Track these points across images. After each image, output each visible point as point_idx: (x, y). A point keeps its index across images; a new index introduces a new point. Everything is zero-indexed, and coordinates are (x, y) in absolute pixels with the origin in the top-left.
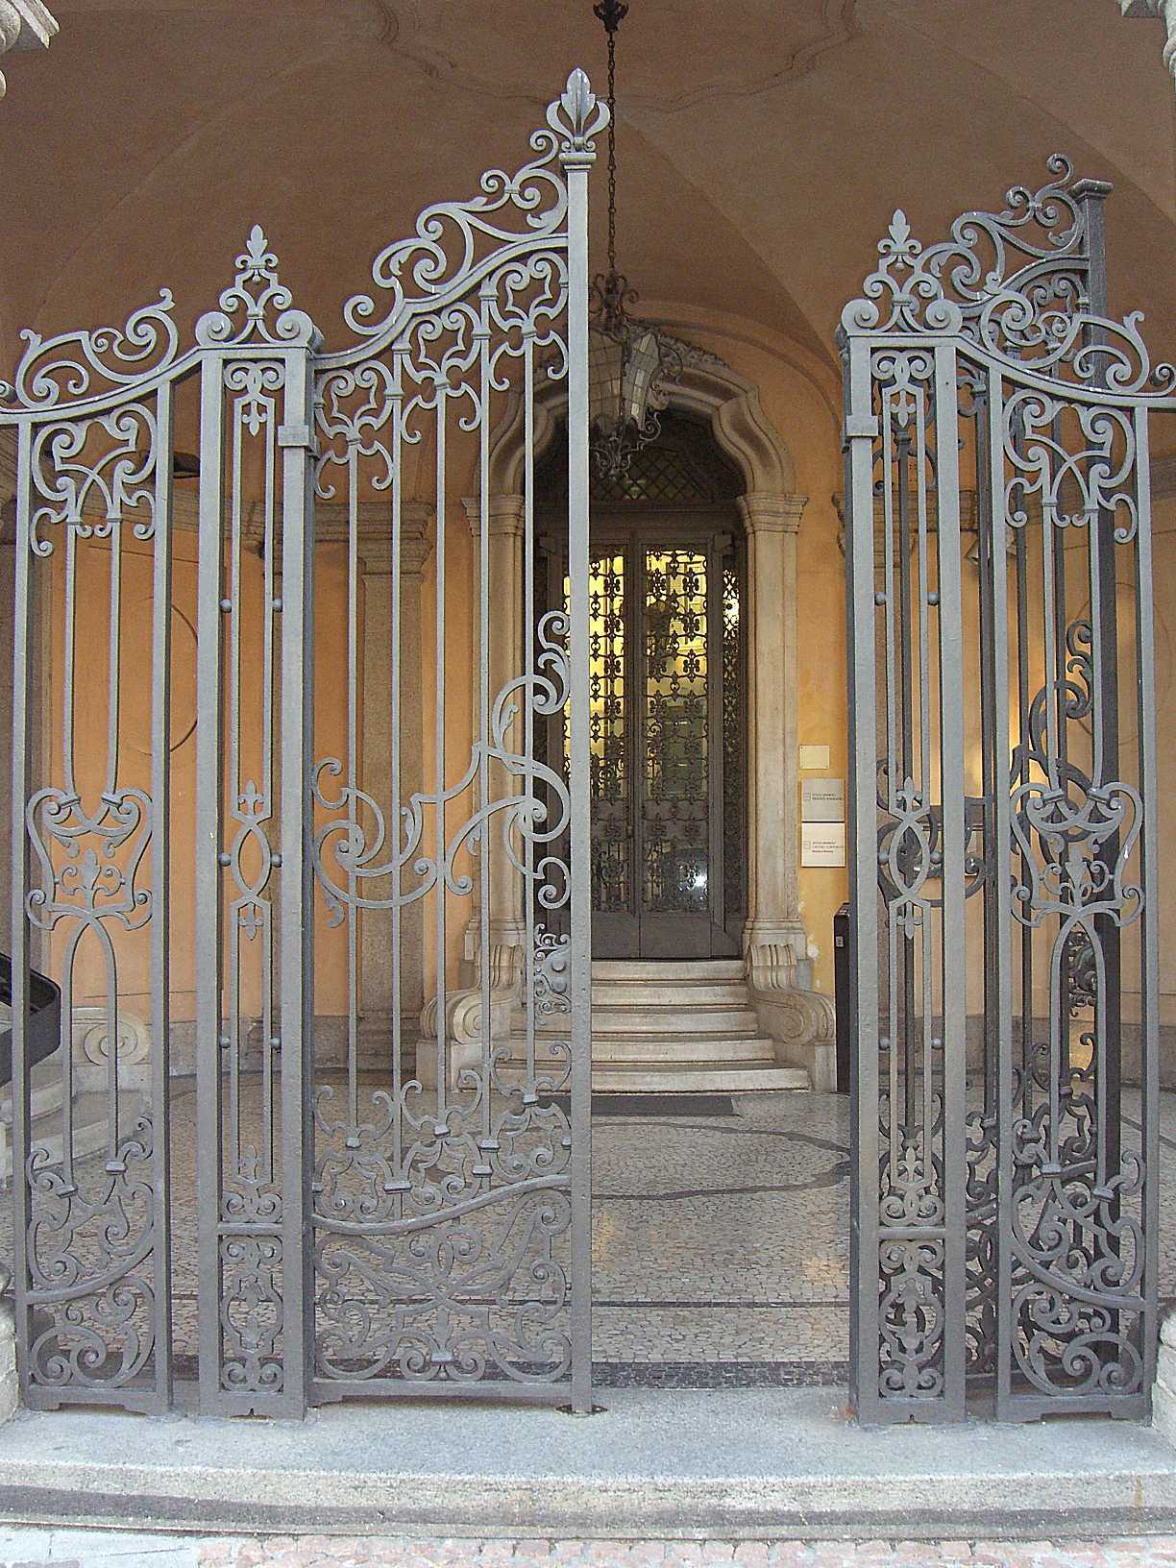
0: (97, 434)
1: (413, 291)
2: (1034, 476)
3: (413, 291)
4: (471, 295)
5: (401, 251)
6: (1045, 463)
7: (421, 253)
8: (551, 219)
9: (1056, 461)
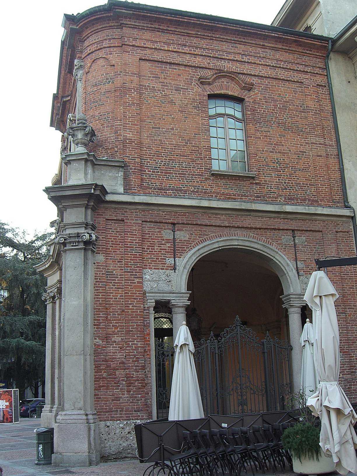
2: (160, 358)
4: (230, 338)
6: (161, 357)
8: (236, 330)
9: (162, 357)
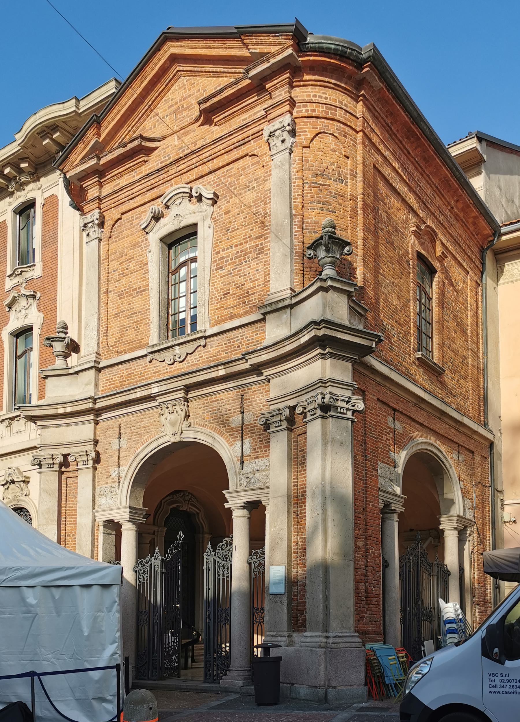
0: (224, 565)
1: (222, 549)
3: (222, 549)
5: (221, 544)
7: (223, 545)
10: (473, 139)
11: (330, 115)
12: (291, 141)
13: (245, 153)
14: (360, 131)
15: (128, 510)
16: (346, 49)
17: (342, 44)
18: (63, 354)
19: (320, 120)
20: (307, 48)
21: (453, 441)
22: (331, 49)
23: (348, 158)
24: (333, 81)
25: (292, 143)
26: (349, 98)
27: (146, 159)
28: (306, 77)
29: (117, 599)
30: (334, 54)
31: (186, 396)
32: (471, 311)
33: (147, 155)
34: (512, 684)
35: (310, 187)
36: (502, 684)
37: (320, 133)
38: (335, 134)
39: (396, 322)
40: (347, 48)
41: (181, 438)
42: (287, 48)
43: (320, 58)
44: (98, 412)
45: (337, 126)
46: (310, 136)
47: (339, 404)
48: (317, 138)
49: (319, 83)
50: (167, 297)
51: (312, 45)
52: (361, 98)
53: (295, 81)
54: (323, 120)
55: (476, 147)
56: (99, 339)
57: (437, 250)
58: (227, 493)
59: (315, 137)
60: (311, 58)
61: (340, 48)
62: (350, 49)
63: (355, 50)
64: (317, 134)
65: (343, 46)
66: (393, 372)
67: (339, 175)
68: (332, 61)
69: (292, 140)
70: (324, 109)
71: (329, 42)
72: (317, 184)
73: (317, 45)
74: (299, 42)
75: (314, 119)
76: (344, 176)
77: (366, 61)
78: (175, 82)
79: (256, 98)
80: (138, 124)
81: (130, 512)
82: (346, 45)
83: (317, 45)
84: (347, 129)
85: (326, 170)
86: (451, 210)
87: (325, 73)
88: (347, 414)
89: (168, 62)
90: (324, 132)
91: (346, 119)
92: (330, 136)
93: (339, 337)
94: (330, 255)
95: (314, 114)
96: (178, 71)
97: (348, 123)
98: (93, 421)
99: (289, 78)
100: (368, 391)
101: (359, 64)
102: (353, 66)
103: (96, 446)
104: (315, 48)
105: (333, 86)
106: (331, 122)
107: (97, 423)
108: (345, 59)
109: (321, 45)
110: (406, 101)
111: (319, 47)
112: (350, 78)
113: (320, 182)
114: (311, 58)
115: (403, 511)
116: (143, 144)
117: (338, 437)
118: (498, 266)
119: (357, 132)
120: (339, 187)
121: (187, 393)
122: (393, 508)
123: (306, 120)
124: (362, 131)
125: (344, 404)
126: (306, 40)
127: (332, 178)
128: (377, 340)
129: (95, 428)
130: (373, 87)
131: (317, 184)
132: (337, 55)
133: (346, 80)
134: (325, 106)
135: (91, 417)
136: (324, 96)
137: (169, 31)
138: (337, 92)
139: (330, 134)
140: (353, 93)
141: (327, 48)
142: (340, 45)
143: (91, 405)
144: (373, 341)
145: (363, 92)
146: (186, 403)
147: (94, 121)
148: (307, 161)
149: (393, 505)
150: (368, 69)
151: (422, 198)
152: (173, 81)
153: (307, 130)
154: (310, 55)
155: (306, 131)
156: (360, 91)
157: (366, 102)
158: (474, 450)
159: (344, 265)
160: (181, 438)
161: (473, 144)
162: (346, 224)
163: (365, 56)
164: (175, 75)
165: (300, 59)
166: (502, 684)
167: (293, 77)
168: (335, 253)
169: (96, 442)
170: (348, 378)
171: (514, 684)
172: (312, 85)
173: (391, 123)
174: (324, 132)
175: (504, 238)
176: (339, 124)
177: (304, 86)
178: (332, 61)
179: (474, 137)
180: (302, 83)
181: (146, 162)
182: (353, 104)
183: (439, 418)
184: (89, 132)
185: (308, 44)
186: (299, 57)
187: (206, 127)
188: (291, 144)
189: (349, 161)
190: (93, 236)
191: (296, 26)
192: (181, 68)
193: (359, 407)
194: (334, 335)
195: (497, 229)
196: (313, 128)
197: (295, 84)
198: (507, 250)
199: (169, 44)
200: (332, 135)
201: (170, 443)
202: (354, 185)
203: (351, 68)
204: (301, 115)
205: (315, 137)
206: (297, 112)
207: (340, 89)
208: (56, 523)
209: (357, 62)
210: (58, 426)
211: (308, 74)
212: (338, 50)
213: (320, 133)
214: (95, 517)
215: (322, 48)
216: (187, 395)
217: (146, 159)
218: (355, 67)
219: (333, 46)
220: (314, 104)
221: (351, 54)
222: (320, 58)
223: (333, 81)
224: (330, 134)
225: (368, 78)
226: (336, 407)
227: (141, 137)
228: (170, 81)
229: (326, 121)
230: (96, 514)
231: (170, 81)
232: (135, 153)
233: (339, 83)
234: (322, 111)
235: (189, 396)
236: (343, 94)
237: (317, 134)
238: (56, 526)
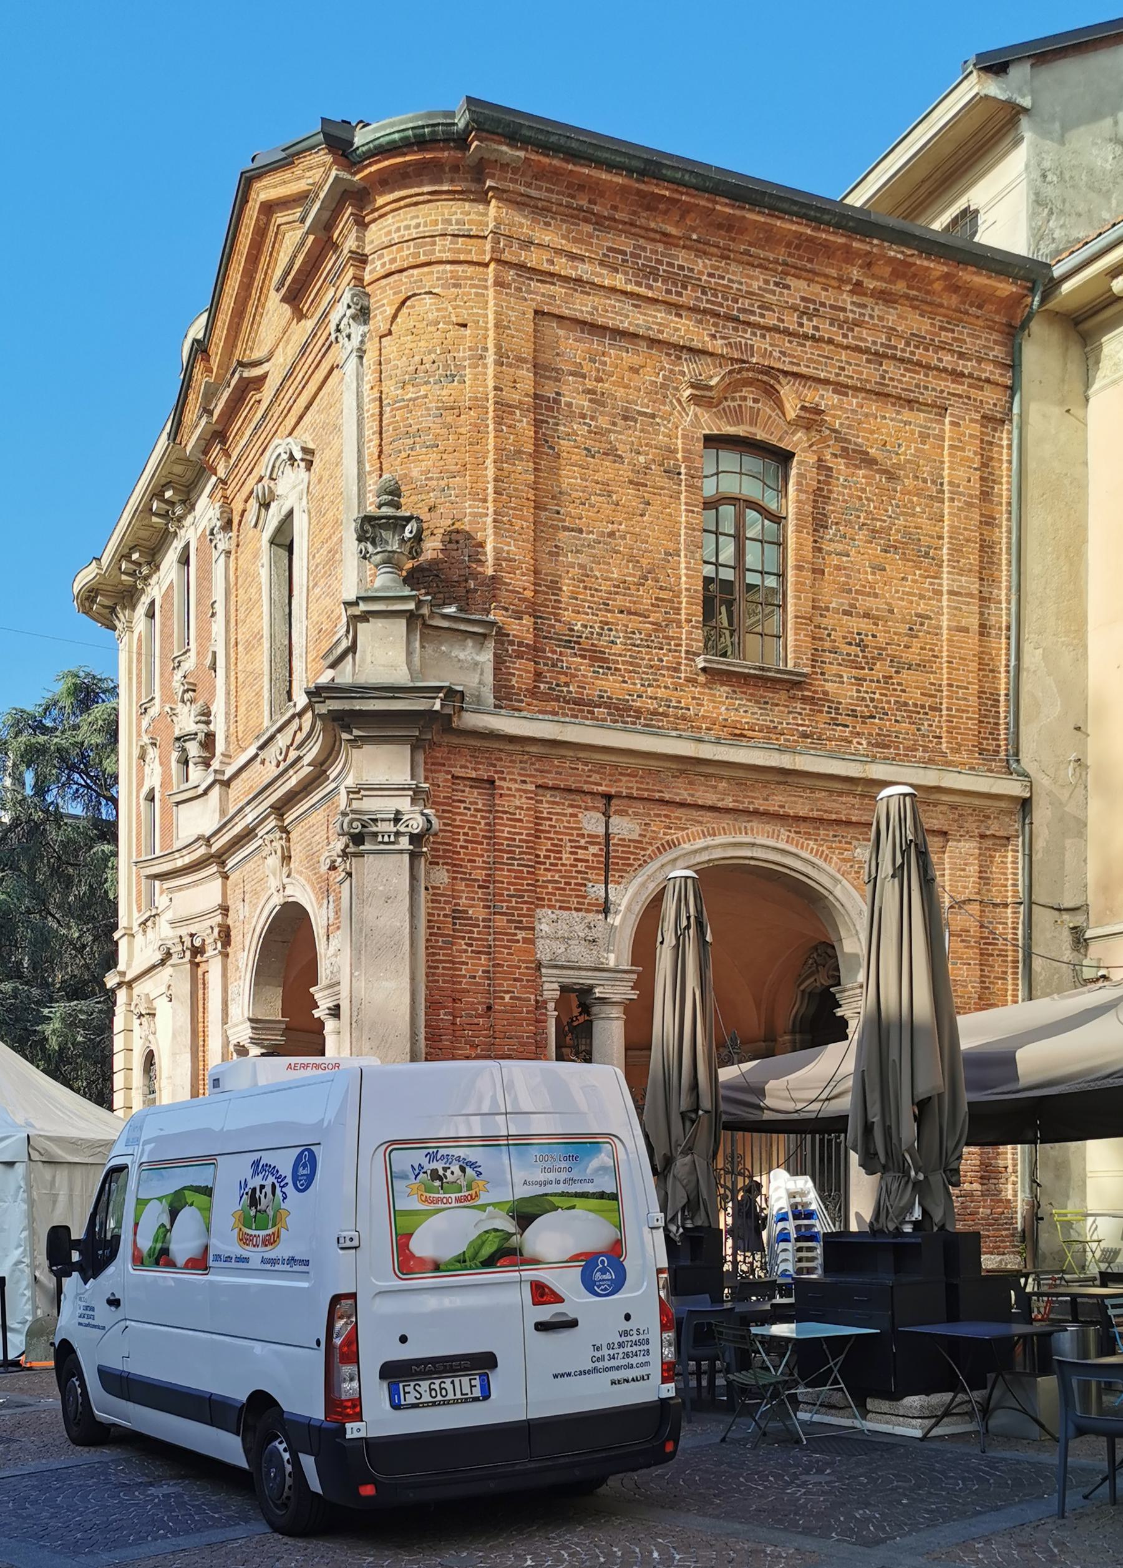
10: (970, 77)
11: (423, 259)
12: (361, 332)
13: (328, 367)
14: (490, 261)
15: (248, 1024)
16: (421, 131)
17: (411, 125)
18: (200, 760)
19: (405, 274)
20: (359, 156)
21: (849, 823)
22: (394, 141)
23: (465, 326)
24: (426, 189)
25: (364, 336)
26: (467, 204)
27: (257, 397)
28: (380, 201)
29: (22, 1184)
30: (406, 146)
31: (280, 824)
32: (952, 500)
33: (258, 389)
34: (626, 1350)
35: (392, 410)
36: (611, 1352)
37: (408, 298)
38: (434, 291)
39: (622, 612)
40: (423, 127)
41: (284, 897)
42: (330, 169)
43: (387, 163)
44: (220, 858)
45: (438, 272)
46: (390, 311)
47: (383, 827)
48: (404, 310)
49: (402, 203)
50: (287, 642)
51: (364, 149)
52: (490, 194)
53: (367, 215)
54: (411, 271)
55: (977, 94)
56: (228, 730)
57: (787, 406)
58: (318, 991)
59: (398, 310)
60: (373, 169)
61: (410, 132)
62: (428, 126)
63: (438, 124)
64: (403, 303)
65: (413, 128)
66: (570, 728)
67: (447, 366)
68: (407, 158)
69: (363, 329)
70: (412, 250)
71: (388, 131)
72: (403, 400)
73: (371, 145)
74: (344, 151)
75: (396, 277)
76: (456, 366)
77: (467, 131)
78: (280, 246)
79: (334, 258)
80: (253, 335)
81: (253, 1028)
82: (420, 123)
83: (371, 145)
84: (459, 268)
85: (419, 367)
86: (858, 289)
87: (407, 181)
88: (398, 843)
89: (262, 217)
90: (415, 295)
91: (459, 251)
92: (427, 296)
93: (358, 708)
94: (379, 549)
95: (393, 267)
96: (279, 226)
97: (462, 257)
98: (218, 875)
99: (352, 214)
100: (500, 779)
101: (461, 141)
102: (449, 149)
103: (227, 915)
104: (369, 150)
105: (429, 197)
106: (426, 269)
107: (226, 877)
108: (429, 146)
109: (377, 142)
110: (599, 154)
111: (375, 148)
112: (455, 168)
113: (410, 395)
114: (373, 169)
115: (635, 997)
116: (245, 375)
117: (381, 888)
118: (1088, 349)
119: (487, 265)
120: (444, 392)
121: (281, 817)
122: (598, 995)
123: (384, 282)
124: (492, 259)
125: (390, 827)
126: (352, 144)
127: (431, 380)
128: (441, 695)
129: (224, 886)
130: (508, 165)
131: (403, 400)
132: (412, 144)
133: (448, 176)
134: (411, 243)
135: (214, 868)
136: (413, 223)
137: (256, 164)
138: (438, 203)
139: (426, 293)
140: (472, 192)
141: (388, 143)
142: (407, 129)
143: (203, 850)
144: (434, 698)
145: (489, 183)
146: (284, 835)
147: (197, 350)
148: (389, 361)
149: (596, 990)
150: (476, 143)
151: (722, 310)
152: (277, 245)
153: (385, 301)
154: (370, 165)
155: (383, 305)
156: (485, 183)
157: (505, 196)
158: (945, 828)
159: (457, 542)
160: (284, 897)
161: (974, 86)
162: (460, 462)
163: (461, 125)
164: (277, 234)
165: (358, 177)
166: (611, 1352)
167: (362, 209)
168: (387, 543)
169: (225, 910)
170: (402, 776)
171: (629, 1349)
172: (393, 211)
173: (590, 202)
174: (415, 295)
175: (1066, 287)
176: (441, 267)
177: (381, 216)
178: (407, 158)
179: (971, 72)
180: (376, 214)
181: (259, 402)
182: (476, 213)
183: (785, 783)
184: (195, 371)
185: (358, 148)
186: (355, 174)
187: (303, 321)
188: (360, 338)
189: (468, 332)
190: (221, 547)
191: (324, 134)
192: (284, 220)
193: (415, 826)
194: (347, 708)
195: (1033, 276)
196: (395, 294)
197: (367, 219)
198: (1095, 309)
199: (257, 185)
200: (430, 293)
201: (278, 908)
202: (482, 376)
203: (446, 154)
204: (376, 276)
205: (398, 310)
206: (371, 272)
207: (444, 197)
208: (189, 1050)
209: (454, 140)
210: (187, 886)
211: (382, 194)
212: (407, 138)
213: (408, 298)
214: (227, 1037)
215: (381, 146)
216: (283, 821)
217: (257, 397)
218: (456, 148)
219: (396, 136)
220: (394, 247)
221: (433, 133)
222: (387, 163)
223: (426, 189)
224: (426, 293)
225: (486, 156)
226: (375, 835)
227: (240, 364)
228: (273, 247)
229: (415, 272)
230: (229, 1033)
231: (273, 247)
232: (243, 391)
233: (436, 188)
234: (408, 256)
235: (286, 822)
236: (451, 203)
237: (403, 303)
238: (189, 1056)
